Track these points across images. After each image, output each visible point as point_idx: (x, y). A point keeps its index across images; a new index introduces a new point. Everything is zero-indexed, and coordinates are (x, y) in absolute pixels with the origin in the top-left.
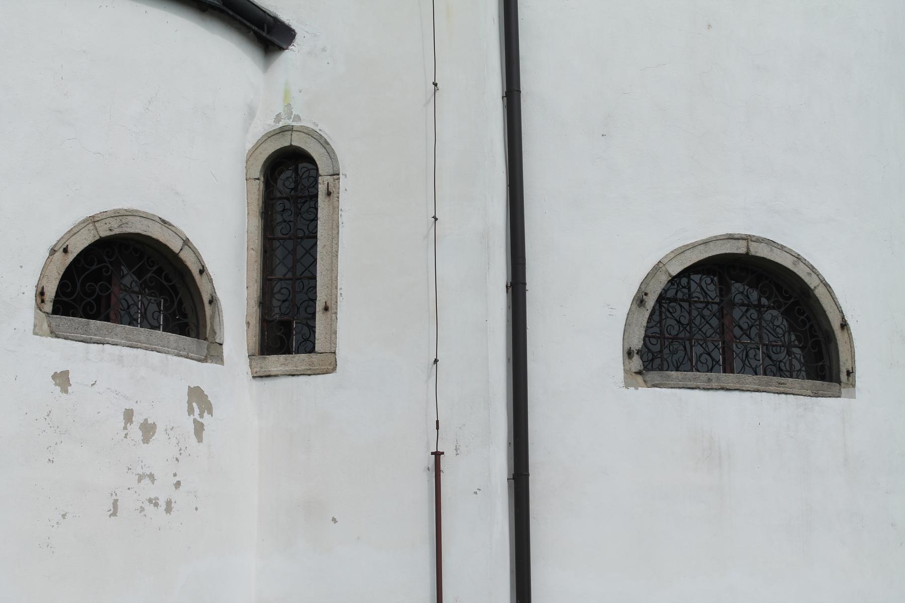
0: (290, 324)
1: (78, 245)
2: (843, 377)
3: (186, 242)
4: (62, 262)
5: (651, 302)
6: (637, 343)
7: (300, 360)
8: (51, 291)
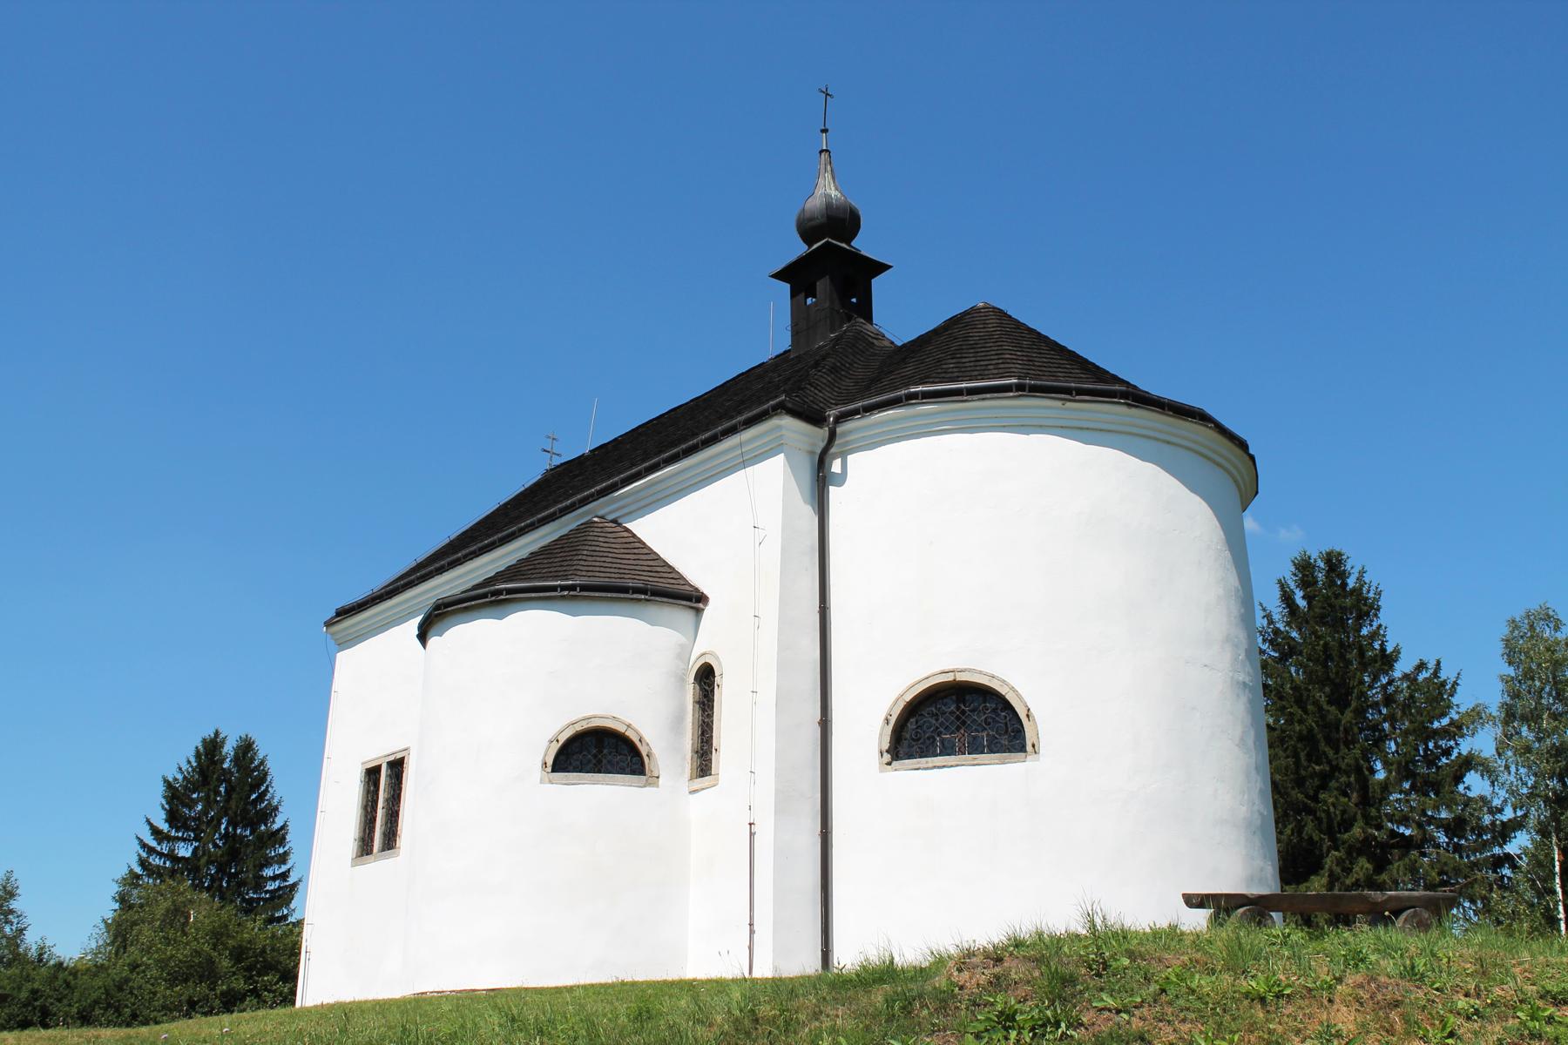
0: (703, 761)
1: (563, 738)
2: (1029, 748)
3: (629, 726)
4: (556, 747)
5: (893, 721)
6: (886, 746)
7: (392, 758)
8: (550, 762)
